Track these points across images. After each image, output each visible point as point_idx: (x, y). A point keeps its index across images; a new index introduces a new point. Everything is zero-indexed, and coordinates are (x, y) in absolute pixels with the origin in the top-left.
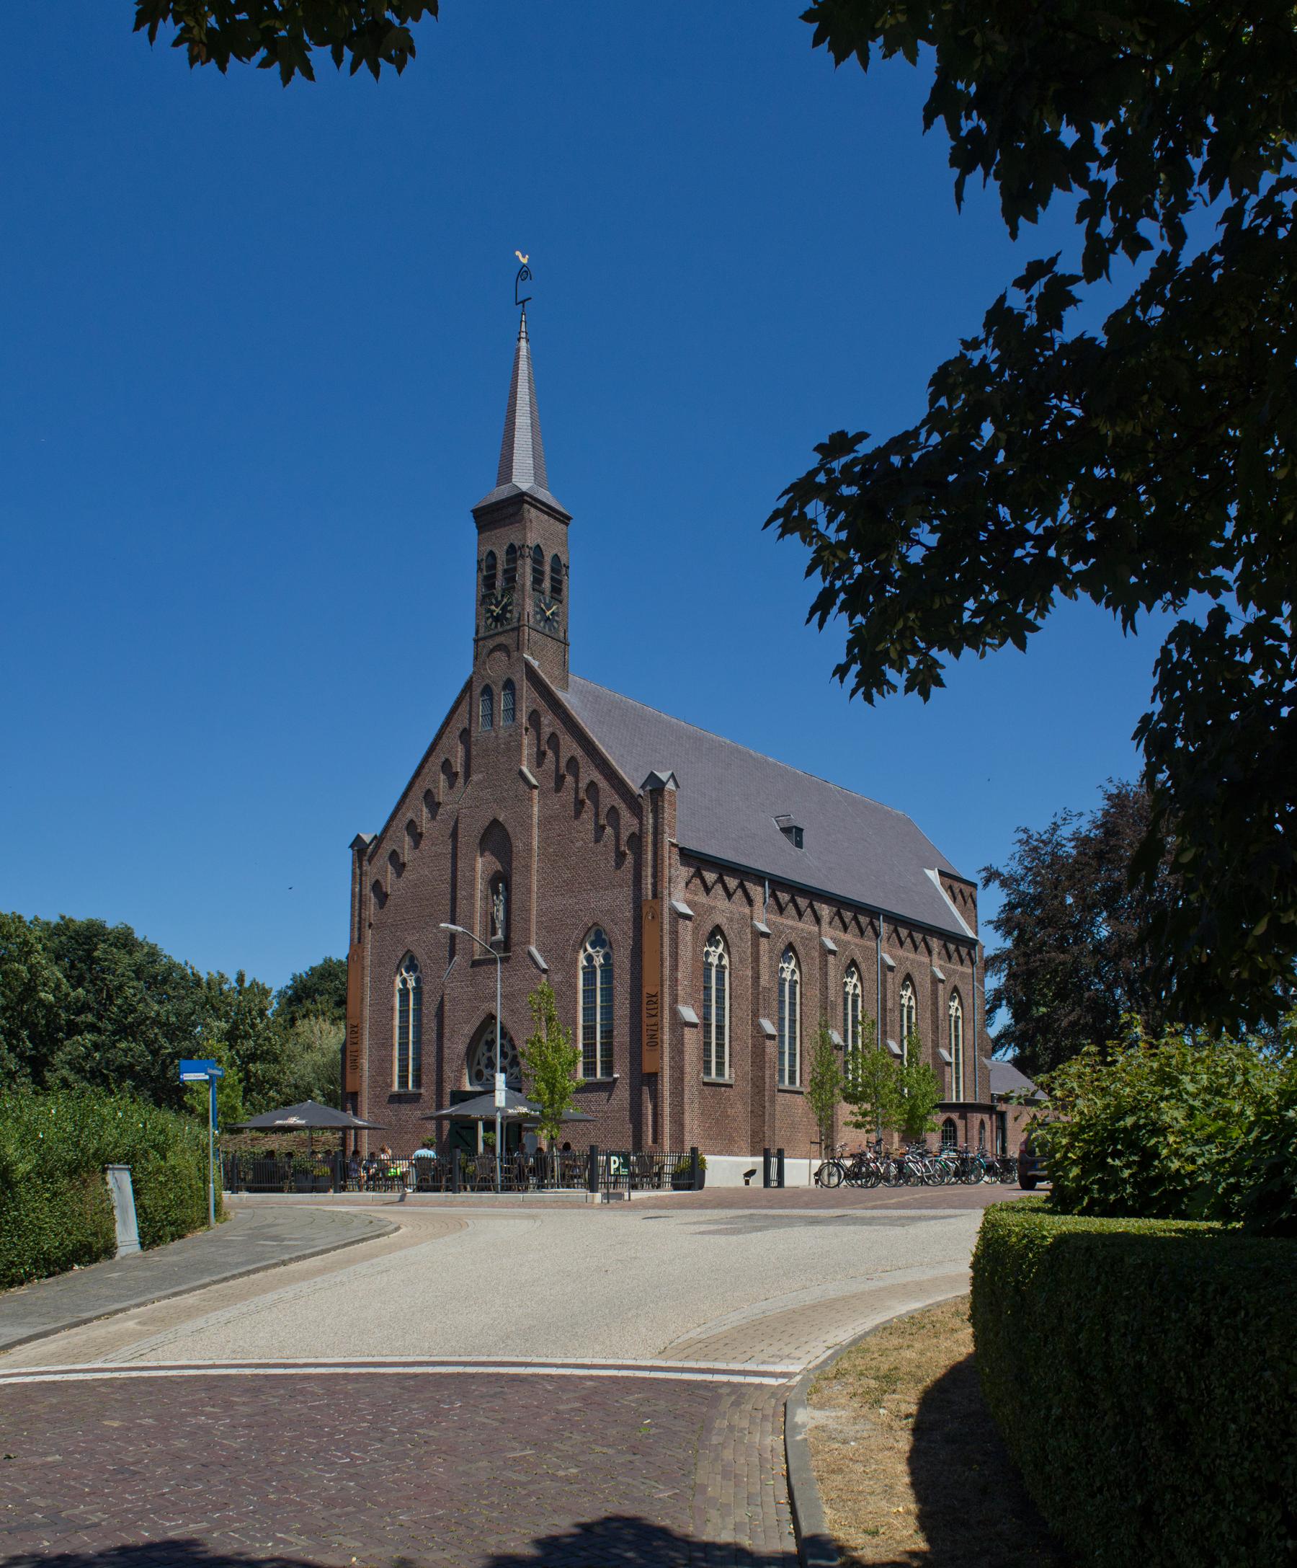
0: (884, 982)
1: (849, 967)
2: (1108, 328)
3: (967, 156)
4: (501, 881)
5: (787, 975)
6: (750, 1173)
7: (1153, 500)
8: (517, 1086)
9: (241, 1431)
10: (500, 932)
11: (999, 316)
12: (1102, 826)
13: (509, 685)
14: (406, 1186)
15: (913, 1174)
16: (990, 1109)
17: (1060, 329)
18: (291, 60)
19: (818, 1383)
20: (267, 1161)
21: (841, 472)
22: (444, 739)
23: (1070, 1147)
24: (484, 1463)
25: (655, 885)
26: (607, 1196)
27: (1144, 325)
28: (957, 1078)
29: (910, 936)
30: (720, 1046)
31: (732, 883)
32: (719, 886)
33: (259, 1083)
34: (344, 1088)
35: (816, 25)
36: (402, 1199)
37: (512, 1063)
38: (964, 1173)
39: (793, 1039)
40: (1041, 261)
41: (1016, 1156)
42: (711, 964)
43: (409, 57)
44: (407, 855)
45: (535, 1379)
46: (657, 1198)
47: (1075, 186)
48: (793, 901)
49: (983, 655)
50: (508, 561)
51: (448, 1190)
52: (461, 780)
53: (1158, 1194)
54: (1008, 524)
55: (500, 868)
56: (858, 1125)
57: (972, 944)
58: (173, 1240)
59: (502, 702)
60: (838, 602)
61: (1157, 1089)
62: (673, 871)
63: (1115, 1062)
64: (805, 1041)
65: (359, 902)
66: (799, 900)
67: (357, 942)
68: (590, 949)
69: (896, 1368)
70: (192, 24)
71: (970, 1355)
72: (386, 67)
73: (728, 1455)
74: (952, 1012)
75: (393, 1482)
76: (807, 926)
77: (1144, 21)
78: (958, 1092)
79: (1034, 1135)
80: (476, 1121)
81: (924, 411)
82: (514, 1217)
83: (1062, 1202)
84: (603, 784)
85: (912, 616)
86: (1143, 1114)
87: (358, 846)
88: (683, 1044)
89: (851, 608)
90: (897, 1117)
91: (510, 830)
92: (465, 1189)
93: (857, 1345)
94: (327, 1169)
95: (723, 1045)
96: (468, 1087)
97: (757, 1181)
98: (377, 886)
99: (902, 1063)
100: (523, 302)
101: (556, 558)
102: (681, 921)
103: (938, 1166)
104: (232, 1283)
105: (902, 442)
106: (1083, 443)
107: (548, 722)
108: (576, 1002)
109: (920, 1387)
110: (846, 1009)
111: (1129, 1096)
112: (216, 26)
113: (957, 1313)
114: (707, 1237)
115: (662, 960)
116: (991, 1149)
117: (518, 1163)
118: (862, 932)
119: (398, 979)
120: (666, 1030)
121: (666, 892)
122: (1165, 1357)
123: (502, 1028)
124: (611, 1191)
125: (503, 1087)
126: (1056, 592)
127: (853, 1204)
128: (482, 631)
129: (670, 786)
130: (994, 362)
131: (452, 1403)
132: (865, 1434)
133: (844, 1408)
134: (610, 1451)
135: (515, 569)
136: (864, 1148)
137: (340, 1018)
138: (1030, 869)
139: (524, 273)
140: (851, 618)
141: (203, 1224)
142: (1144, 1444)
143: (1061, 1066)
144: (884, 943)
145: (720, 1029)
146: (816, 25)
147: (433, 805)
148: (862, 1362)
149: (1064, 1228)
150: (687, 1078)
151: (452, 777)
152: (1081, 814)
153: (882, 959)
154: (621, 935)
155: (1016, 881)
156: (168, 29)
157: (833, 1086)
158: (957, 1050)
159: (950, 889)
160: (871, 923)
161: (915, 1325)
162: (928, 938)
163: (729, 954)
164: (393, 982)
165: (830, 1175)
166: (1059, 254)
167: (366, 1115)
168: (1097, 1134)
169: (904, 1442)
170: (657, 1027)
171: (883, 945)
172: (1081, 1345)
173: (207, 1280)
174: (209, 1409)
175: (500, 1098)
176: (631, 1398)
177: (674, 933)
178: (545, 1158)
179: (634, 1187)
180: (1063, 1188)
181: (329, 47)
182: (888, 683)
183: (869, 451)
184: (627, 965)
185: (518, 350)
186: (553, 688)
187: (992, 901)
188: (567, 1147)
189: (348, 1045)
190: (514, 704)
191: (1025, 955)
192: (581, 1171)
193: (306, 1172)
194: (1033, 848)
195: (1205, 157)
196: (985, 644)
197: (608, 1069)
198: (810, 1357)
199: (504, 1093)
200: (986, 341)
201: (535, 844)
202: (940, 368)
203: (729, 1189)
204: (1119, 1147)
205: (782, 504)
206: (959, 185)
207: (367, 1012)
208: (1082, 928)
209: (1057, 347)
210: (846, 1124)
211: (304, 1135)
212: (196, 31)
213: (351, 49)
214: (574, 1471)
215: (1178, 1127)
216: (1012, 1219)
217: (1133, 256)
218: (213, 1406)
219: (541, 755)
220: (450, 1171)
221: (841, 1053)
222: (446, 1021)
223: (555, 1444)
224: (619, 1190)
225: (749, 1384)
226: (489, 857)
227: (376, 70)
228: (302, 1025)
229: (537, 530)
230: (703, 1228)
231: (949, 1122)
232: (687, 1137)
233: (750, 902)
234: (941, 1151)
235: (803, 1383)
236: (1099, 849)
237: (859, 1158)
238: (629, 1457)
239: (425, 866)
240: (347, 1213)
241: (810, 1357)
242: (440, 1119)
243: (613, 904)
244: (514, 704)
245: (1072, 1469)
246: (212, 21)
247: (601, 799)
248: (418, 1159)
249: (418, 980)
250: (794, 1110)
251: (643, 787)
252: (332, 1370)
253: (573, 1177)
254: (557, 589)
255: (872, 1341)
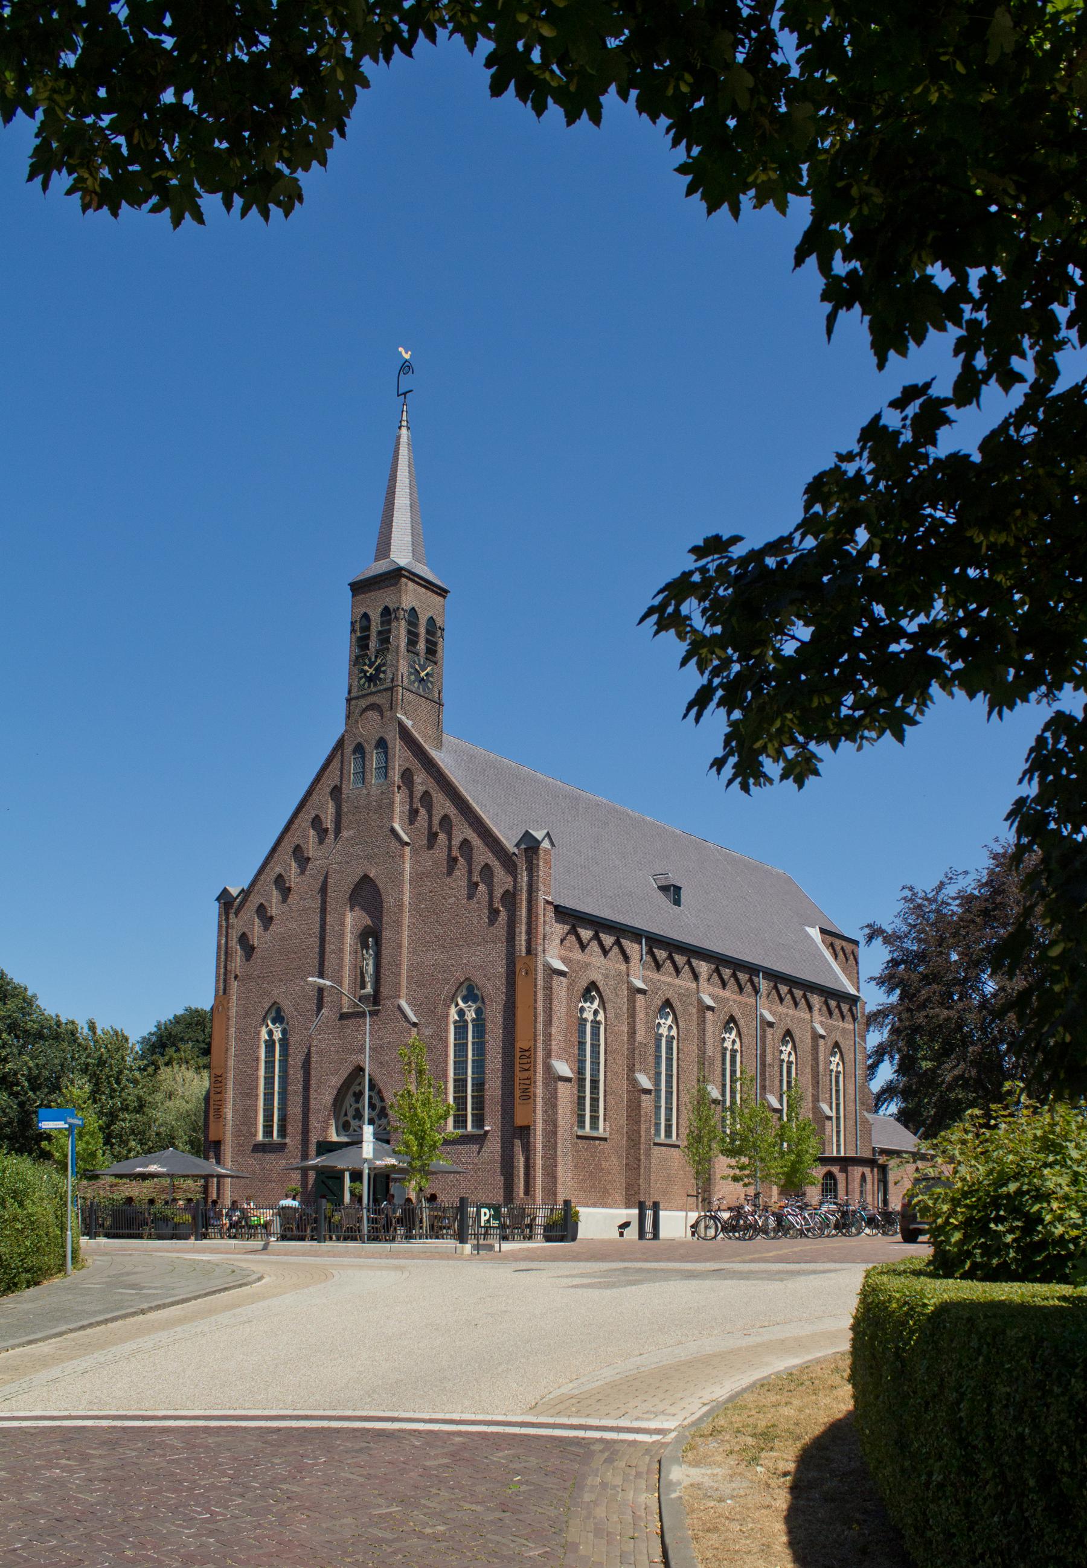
0: (763, 1038)
1: (728, 1023)
2: (982, 448)
3: (839, 295)
4: (371, 936)
5: (664, 1031)
6: (626, 1225)
7: (1027, 600)
8: (385, 1137)
9: (97, 1485)
10: (369, 985)
11: (874, 434)
12: (986, 884)
13: (382, 744)
14: (269, 1234)
15: (791, 1226)
16: (871, 1163)
17: (934, 444)
18: (182, 206)
19: (694, 1440)
20: (126, 1207)
21: (716, 571)
22: (314, 796)
23: (953, 1212)
24: (349, 1520)
25: (529, 942)
26: (477, 1247)
27: (1018, 443)
28: (838, 1132)
29: (791, 992)
30: (595, 1100)
31: (608, 940)
32: (595, 943)
33: (123, 1129)
34: (206, 1136)
35: (690, 177)
36: (265, 1248)
37: (380, 1114)
38: (845, 1226)
39: (669, 1093)
40: (916, 386)
41: (898, 1208)
42: (585, 1020)
43: (297, 203)
44: (275, 908)
45: (402, 1435)
46: (528, 1249)
47: (949, 325)
48: (670, 958)
49: (860, 748)
50: (382, 623)
51: (312, 1239)
52: (331, 836)
53: (1042, 1260)
54: (883, 620)
55: (369, 922)
56: (736, 1179)
57: (854, 1000)
58: (28, 1287)
59: (374, 759)
60: (716, 699)
61: (1041, 1156)
62: (547, 928)
63: (996, 1127)
64: (682, 1095)
65: (225, 954)
66: (677, 957)
67: (223, 993)
68: (461, 1004)
69: (773, 1426)
70: (86, 175)
71: (850, 1413)
72: (275, 211)
73: (600, 1512)
74: (833, 1067)
75: (255, 1539)
76: (685, 982)
77: (1015, 178)
78: (838, 1146)
79: (915, 1200)
80: (342, 1171)
81: (799, 516)
82: (381, 1268)
83: (944, 1265)
84: (476, 841)
85: (789, 716)
86: (1026, 1180)
87: (225, 900)
88: (556, 1098)
89: (729, 703)
90: (776, 1168)
91: (381, 886)
92: (331, 1239)
93: (734, 1401)
94: (188, 1217)
95: (597, 1100)
96: (334, 1138)
97: (632, 1233)
98: (243, 939)
99: (780, 1119)
100: (405, 394)
101: (431, 620)
102: (555, 977)
103: (818, 1219)
104: (89, 1331)
105: (778, 546)
106: (955, 546)
107: (421, 779)
108: (447, 1055)
109: (799, 1445)
110: (724, 1063)
111: (1012, 1162)
112: (109, 177)
113: (837, 1370)
114: (580, 1291)
115: (535, 1015)
116: (873, 1202)
117: (389, 1214)
118: (741, 989)
119: (264, 1030)
120: (539, 1084)
121: (540, 949)
122: (1048, 1431)
123: (370, 1080)
124: (481, 1242)
125: (371, 1139)
126: (935, 689)
127: (730, 1257)
128: (355, 690)
129: (546, 844)
130: (869, 473)
131: (316, 1458)
132: (742, 1493)
133: (720, 1466)
134: (479, 1508)
135: (389, 631)
136: (742, 1201)
137: (205, 1067)
138: (915, 926)
139: (406, 367)
140: (729, 713)
141: (60, 1271)
142: (1026, 1514)
143: (943, 1134)
144: (764, 999)
145: (595, 1083)
146: (690, 177)
147: (302, 860)
148: (738, 1419)
149: (946, 1296)
150: (561, 1132)
151: (322, 833)
152: (966, 873)
153: (761, 1015)
154: (494, 989)
155: (899, 937)
156: (62, 180)
157: (710, 1140)
158: (838, 1105)
159: (832, 946)
160: (751, 981)
161: (793, 1382)
162: (809, 995)
163: (605, 1009)
164: (258, 1033)
165: (707, 1227)
166: (933, 379)
167: (229, 1164)
168: (979, 1199)
169: (782, 1501)
170: (530, 1082)
171: (763, 1001)
172: (962, 1414)
173: (64, 1328)
174: (64, 1461)
175: (368, 1149)
176: (501, 1454)
177: (548, 988)
178: (413, 1210)
179: (505, 1238)
180: (945, 1252)
181: (220, 194)
182: (765, 776)
183: (743, 553)
184: (500, 1019)
185: (399, 437)
186: (426, 747)
187: (875, 958)
188: (433, 1198)
189: (212, 1095)
190: (386, 762)
191: (909, 1010)
192: (453, 1223)
193: (166, 1219)
194: (916, 905)
195: (1072, 306)
196: (862, 738)
197: (479, 1121)
198: (685, 1414)
199: (371, 1146)
200: (860, 454)
201: (406, 899)
202: (815, 478)
203: (602, 1241)
204: (1002, 1213)
205: (656, 602)
206: (831, 319)
207: (231, 1063)
208: (968, 983)
209: (931, 462)
210: (723, 1178)
211: (166, 1182)
212: (90, 182)
213: (241, 196)
214: (441, 1528)
215: (1061, 1193)
216: (895, 1285)
217: (1006, 388)
218: (69, 1459)
219: (413, 813)
220: (316, 1221)
221: (719, 1107)
222: (313, 1072)
223: (423, 1501)
224: (489, 1242)
225: (622, 1441)
226: (359, 912)
227: (265, 214)
228: (165, 1073)
229: (410, 596)
230: (577, 1281)
231: (829, 1175)
232: (560, 1189)
233: (627, 959)
234: (821, 1203)
235: (677, 1440)
236: (984, 907)
237: (738, 1211)
238: (499, 1514)
239: (294, 920)
240: (209, 1262)
241: (685, 1414)
242: (305, 1171)
243: (486, 960)
244: (386, 762)
245: (954, 1535)
246: (105, 173)
247: (475, 856)
248: (283, 1208)
249: (284, 1032)
250: (670, 1164)
251: (517, 845)
252: (192, 1423)
253: (441, 1228)
254: (432, 650)
255: (749, 1397)
